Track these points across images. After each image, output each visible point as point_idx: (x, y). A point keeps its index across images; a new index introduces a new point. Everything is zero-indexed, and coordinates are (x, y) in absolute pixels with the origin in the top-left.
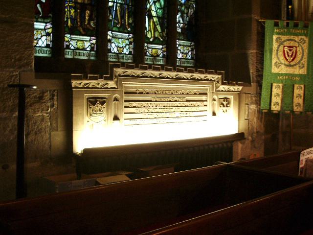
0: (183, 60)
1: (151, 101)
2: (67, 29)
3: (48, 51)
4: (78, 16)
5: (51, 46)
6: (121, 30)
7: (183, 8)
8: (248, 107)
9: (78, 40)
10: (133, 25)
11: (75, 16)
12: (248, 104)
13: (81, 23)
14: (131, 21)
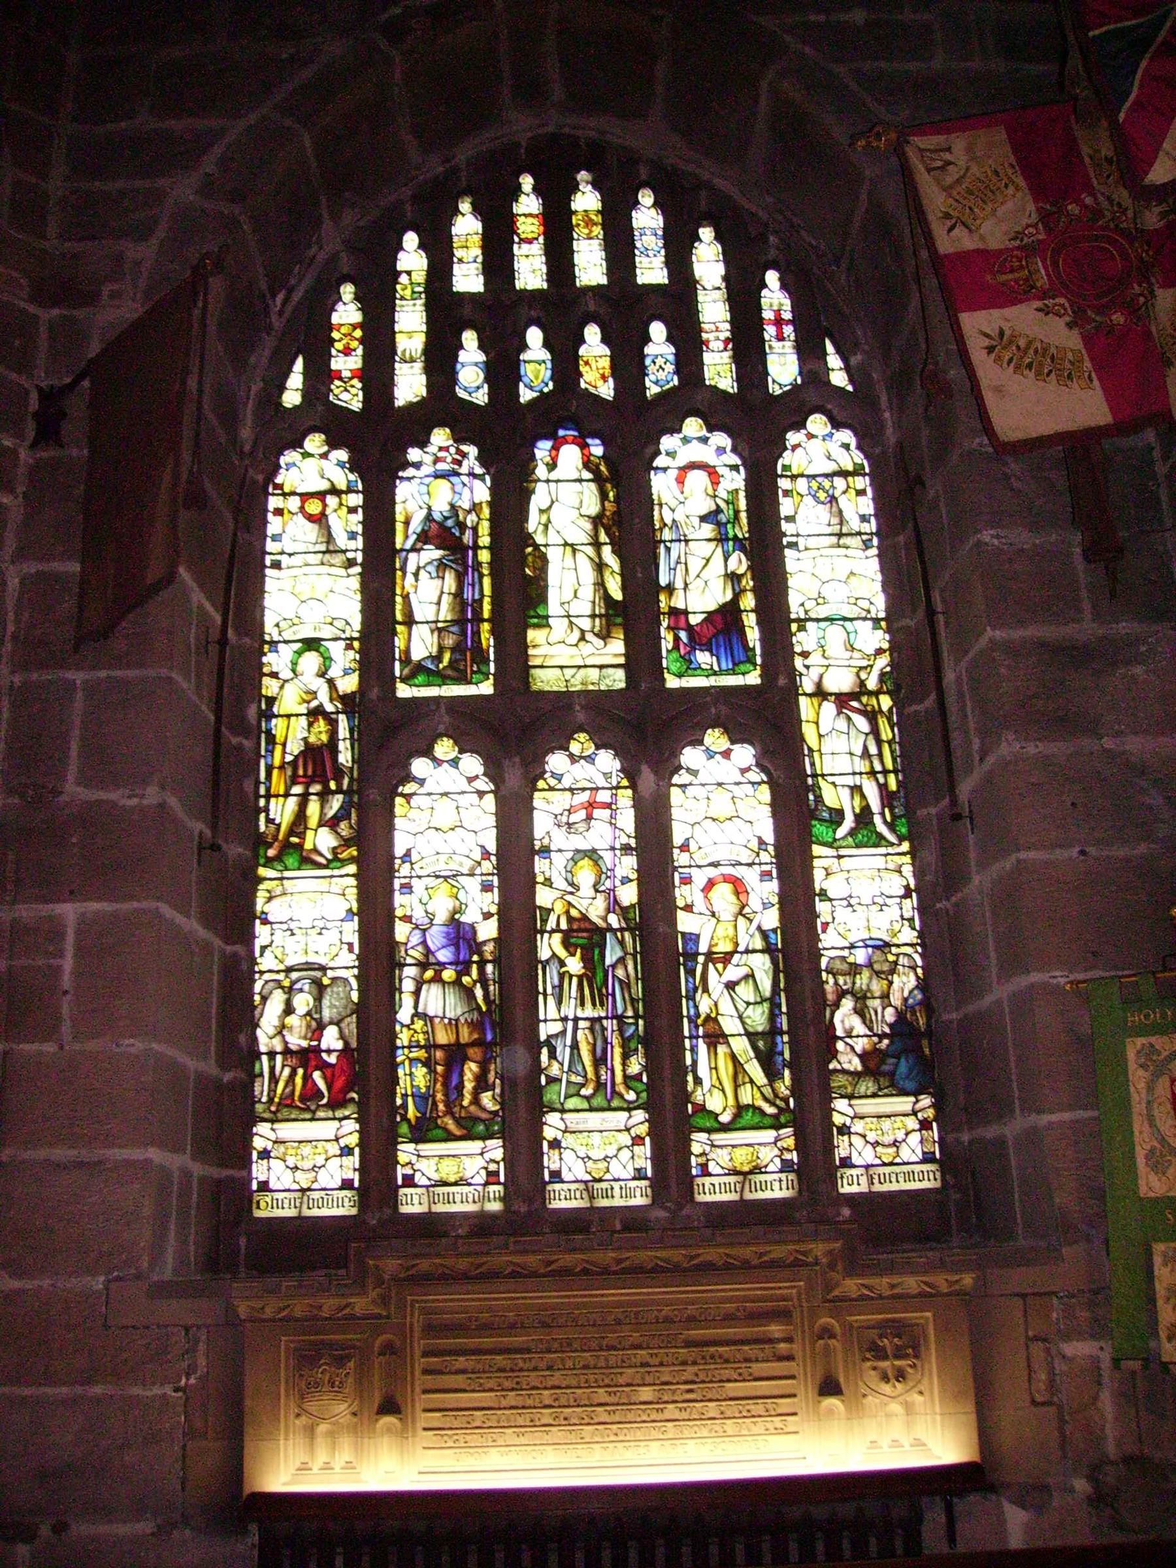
0: (881, 1170)
1: (529, 1351)
2: (404, 1129)
3: (346, 1200)
4: (439, 1086)
5: (938, 1156)
6: (599, 1101)
7: (862, 980)
8: (1048, 1351)
9: (441, 1157)
10: (645, 1079)
11: (428, 1088)
12: (1045, 1340)
13: (447, 1104)
14: (635, 1067)
